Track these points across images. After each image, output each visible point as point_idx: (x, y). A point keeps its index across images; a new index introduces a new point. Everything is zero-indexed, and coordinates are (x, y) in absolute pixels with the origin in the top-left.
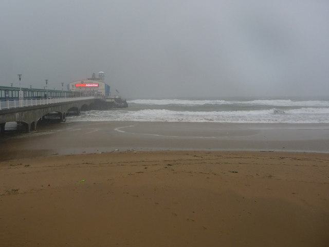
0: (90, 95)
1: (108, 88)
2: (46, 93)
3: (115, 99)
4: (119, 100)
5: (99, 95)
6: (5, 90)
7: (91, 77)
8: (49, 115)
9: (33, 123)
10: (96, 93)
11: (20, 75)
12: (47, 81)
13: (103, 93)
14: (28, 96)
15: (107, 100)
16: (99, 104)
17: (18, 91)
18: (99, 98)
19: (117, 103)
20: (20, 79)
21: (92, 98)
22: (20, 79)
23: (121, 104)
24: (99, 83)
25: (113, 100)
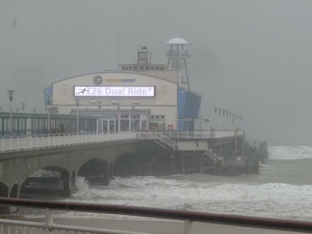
0: (124, 126)
1: (190, 104)
2: (63, 122)
3: (211, 141)
4: (234, 145)
5: (153, 126)
6: (32, 118)
7: (134, 61)
8: (29, 180)
9: (16, 186)
10: (143, 118)
11: (11, 92)
12: (11, 92)
13: (171, 118)
14: (57, 121)
15: (183, 147)
16: (152, 156)
17: (26, 118)
18: (151, 135)
19: (215, 157)
20: (11, 99)
21: (129, 135)
22: (11, 99)
23: (238, 158)
24: (160, 83)
25: (203, 146)
